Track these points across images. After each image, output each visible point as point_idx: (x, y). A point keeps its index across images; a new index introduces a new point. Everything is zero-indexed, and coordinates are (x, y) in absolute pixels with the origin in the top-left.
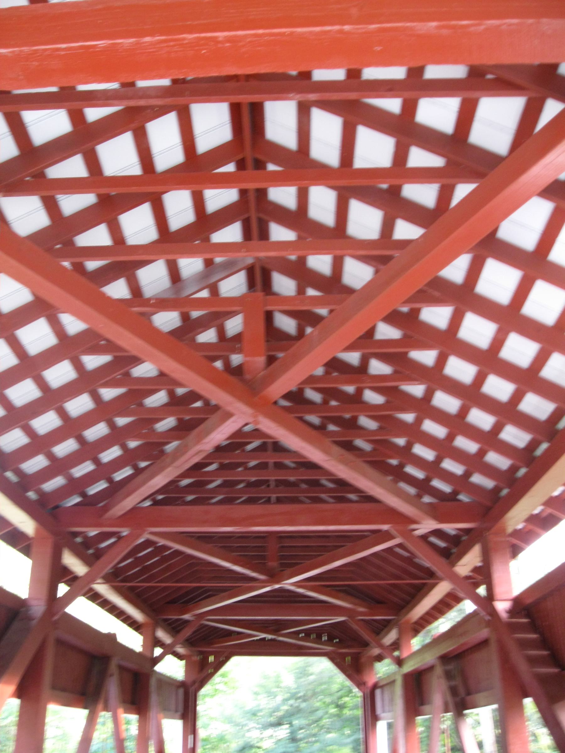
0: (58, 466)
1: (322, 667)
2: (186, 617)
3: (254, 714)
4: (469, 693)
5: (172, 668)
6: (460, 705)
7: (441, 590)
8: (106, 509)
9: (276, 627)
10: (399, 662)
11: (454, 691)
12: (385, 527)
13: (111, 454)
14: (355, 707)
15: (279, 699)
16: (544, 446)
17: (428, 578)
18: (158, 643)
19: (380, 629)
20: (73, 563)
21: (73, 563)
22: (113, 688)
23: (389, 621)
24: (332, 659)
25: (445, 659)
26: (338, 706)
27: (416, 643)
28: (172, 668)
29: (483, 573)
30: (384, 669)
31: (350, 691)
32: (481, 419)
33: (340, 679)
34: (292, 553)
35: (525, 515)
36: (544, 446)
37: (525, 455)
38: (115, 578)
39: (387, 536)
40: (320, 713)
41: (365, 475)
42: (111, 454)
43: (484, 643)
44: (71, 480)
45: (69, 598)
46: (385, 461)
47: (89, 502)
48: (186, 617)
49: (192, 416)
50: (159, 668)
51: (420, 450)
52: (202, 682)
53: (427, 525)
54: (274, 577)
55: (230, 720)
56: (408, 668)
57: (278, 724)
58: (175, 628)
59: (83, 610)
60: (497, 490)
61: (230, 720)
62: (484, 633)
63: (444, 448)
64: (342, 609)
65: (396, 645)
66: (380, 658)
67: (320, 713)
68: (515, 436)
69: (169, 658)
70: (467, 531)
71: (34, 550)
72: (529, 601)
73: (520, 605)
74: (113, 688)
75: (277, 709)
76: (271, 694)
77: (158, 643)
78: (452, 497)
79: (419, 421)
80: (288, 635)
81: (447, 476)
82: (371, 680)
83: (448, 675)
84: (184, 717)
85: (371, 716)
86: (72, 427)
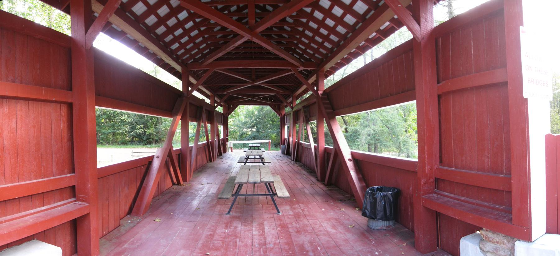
0: (182, 46)
1: (268, 108)
2: (225, 93)
3: (245, 124)
4: (310, 117)
5: (219, 109)
6: (307, 120)
7: (304, 87)
8: (202, 63)
9: (254, 96)
10: (292, 108)
11: (306, 116)
12: (289, 68)
13: (194, 33)
14: (278, 121)
15: (253, 119)
16: (343, 42)
17: (300, 85)
18: (216, 102)
19: (287, 97)
20: (192, 80)
21: (192, 80)
22: (204, 116)
23: (289, 95)
24: (271, 107)
25: (304, 107)
26: (272, 121)
27: (298, 102)
28: (219, 109)
29: (316, 83)
30: (287, 110)
31: (277, 116)
32: (330, 22)
33: (273, 112)
34: (260, 74)
35: (330, 66)
36: (343, 42)
37: (343, 37)
38: (205, 85)
39: (290, 71)
40: (267, 123)
41: (283, 54)
42: (194, 33)
43: (315, 103)
44: (191, 55)
45: (192, 91)
46: (290, 49)
47: (196, 61)
48: (225, 93)
49: (229, 36)
50: (217, 109)
51: (307, 33)
52: (229, 113)
53: (301, 68)
54: (254, 81)
55: (237, 126)
56: (294, 110)
57: (253, 127)
58: (220, 97)
59: (196, 94)
60: (322, 59)
61: (237, 126)
62: (315, 100)
63: (308, 46)
64: (275, 91)
65: (292, 102)
66: (286, 106)
67: (267, 123)
68: (350, 19)
69: (219, 107)
70: (313, 70)
71: (72, 10)
72: (328, 91)
73: (325, 92)
74: (204, 116)
75: (253, 122)
76: (251, 118)
77: (216, 102)
78: (309, 60)
79: (313, 12)
80: (257, 99)
81: (308, 54)
82: (283, 113)
83: (305, 112)
84: (223, 125)
85: (283, 124)
86: (192, 40)
